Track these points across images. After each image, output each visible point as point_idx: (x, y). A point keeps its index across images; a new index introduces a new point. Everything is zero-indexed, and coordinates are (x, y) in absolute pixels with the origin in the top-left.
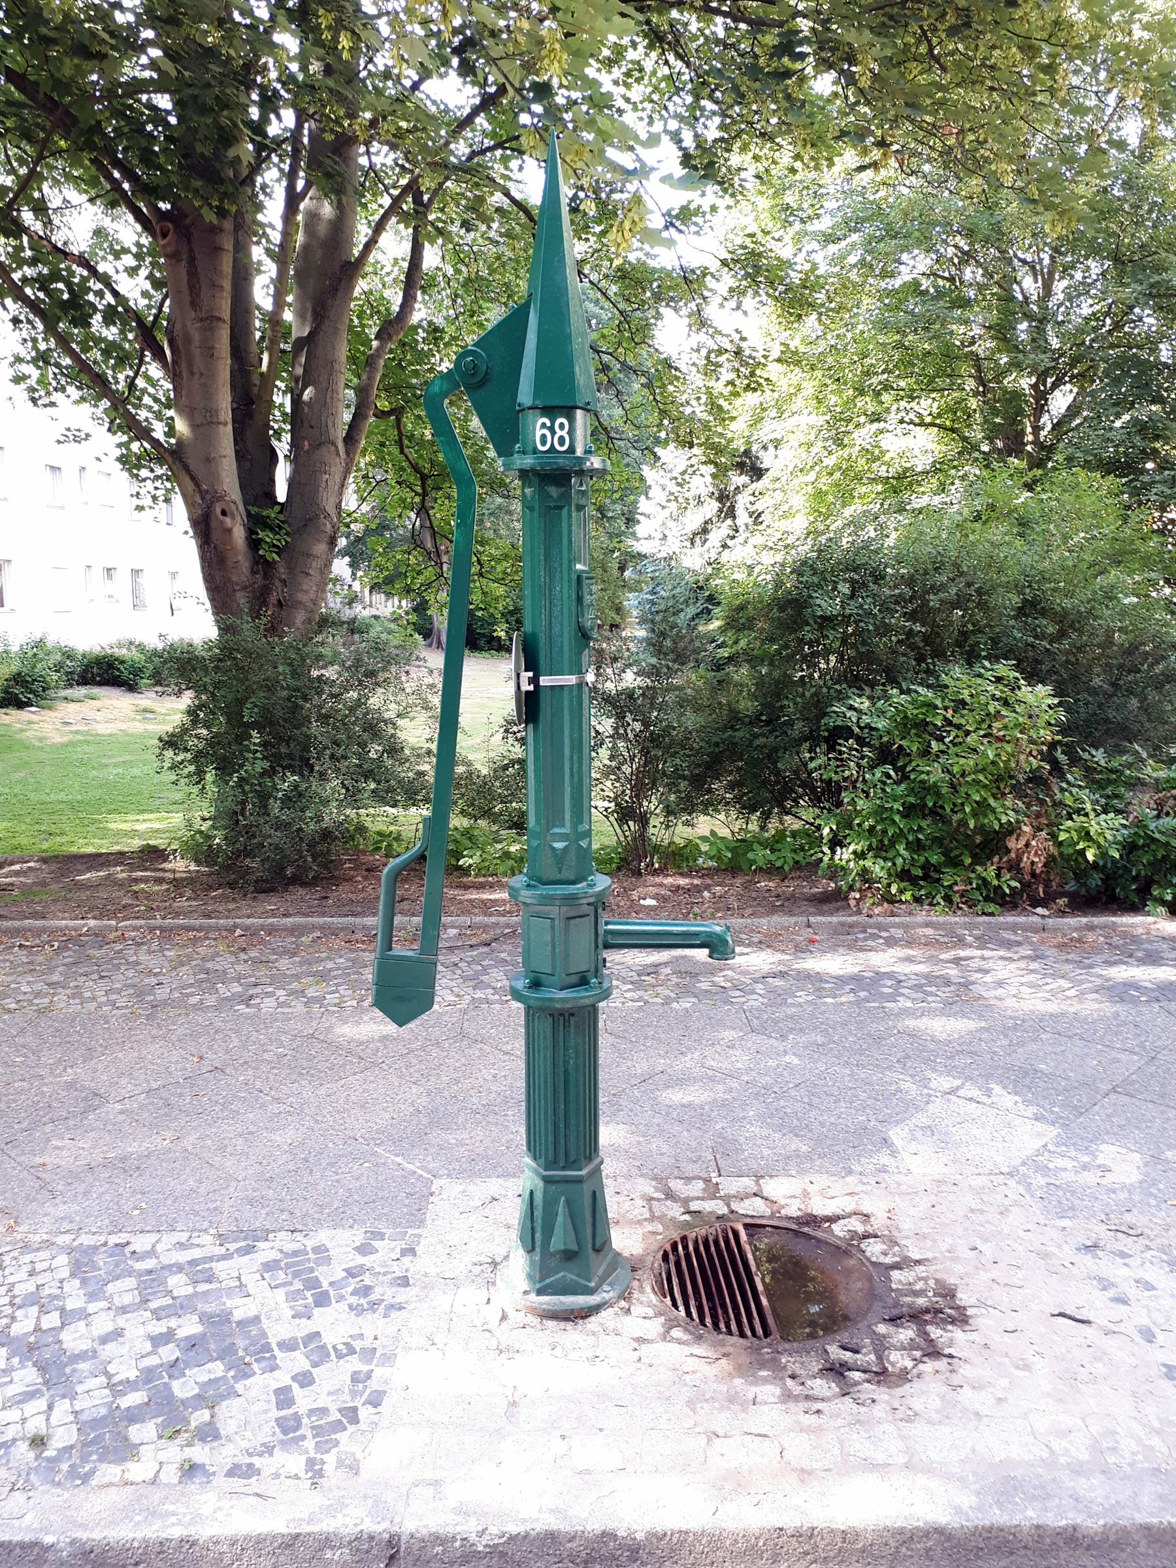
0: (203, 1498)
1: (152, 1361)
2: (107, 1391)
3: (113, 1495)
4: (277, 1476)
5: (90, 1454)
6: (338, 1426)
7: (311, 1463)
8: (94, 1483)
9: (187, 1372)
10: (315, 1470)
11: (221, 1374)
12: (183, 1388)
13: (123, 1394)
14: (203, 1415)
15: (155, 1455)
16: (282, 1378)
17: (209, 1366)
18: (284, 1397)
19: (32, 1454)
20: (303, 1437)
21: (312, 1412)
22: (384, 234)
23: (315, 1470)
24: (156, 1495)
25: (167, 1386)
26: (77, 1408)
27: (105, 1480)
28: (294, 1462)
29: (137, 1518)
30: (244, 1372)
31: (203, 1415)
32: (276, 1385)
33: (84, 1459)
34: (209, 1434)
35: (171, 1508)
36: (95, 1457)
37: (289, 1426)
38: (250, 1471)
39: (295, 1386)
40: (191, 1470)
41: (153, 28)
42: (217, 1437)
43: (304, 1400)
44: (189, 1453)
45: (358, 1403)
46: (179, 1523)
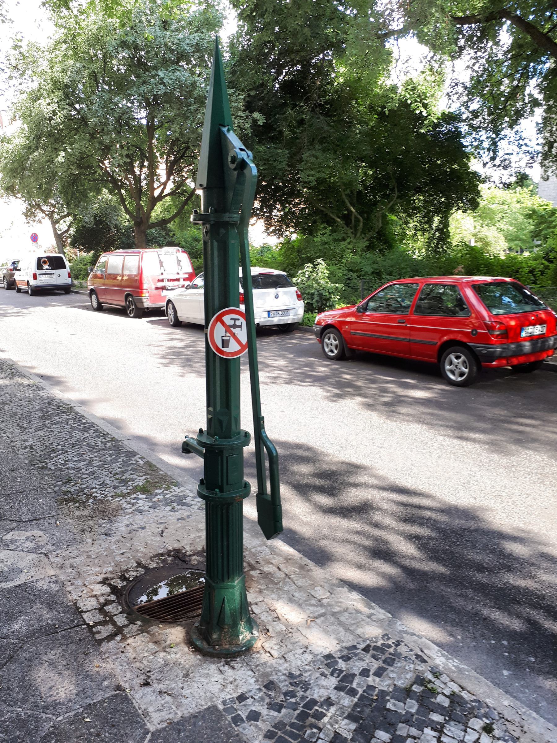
0: (440, 663)
1: (414, 731)
2: (445, 731)
3: (469, 687)
4: (411, 650)
5: (469, 708)
6: (376, 648)
7: (397, 645)
8: (474, 697)
9: (404, 713)
10: (398, 644)
11: (392, 701)
12: (412, 706)
13: (438, 723)
14: (415, 688)
15: (446, 687)
16: (371, 680)
17: (393, 708)
18: (379, 673)
19: (494, 726)
20: (390, 654)
21: (377, 659)
22: (204, 346)
23: (398, 644)
24: (454, 675)
25: (417, 713)
26: (463, 733)
27: (469, 695)
28: (402, 649)
29: (467, 673)
30: (383, 694)
31: (415, 688)
32: (377, 679)
33: (473, 708)
34: (420, 680)
35: (453, 668)
36: (469, 706)
37: (390, 662)
38: (418, 656)
39: (371, 673)
40: (437, 674)
41: (243, 225)
42: (418, 677)
43: (375, 665)
44: (433, 679)
45: (360, 651)
46: (454, 662)
